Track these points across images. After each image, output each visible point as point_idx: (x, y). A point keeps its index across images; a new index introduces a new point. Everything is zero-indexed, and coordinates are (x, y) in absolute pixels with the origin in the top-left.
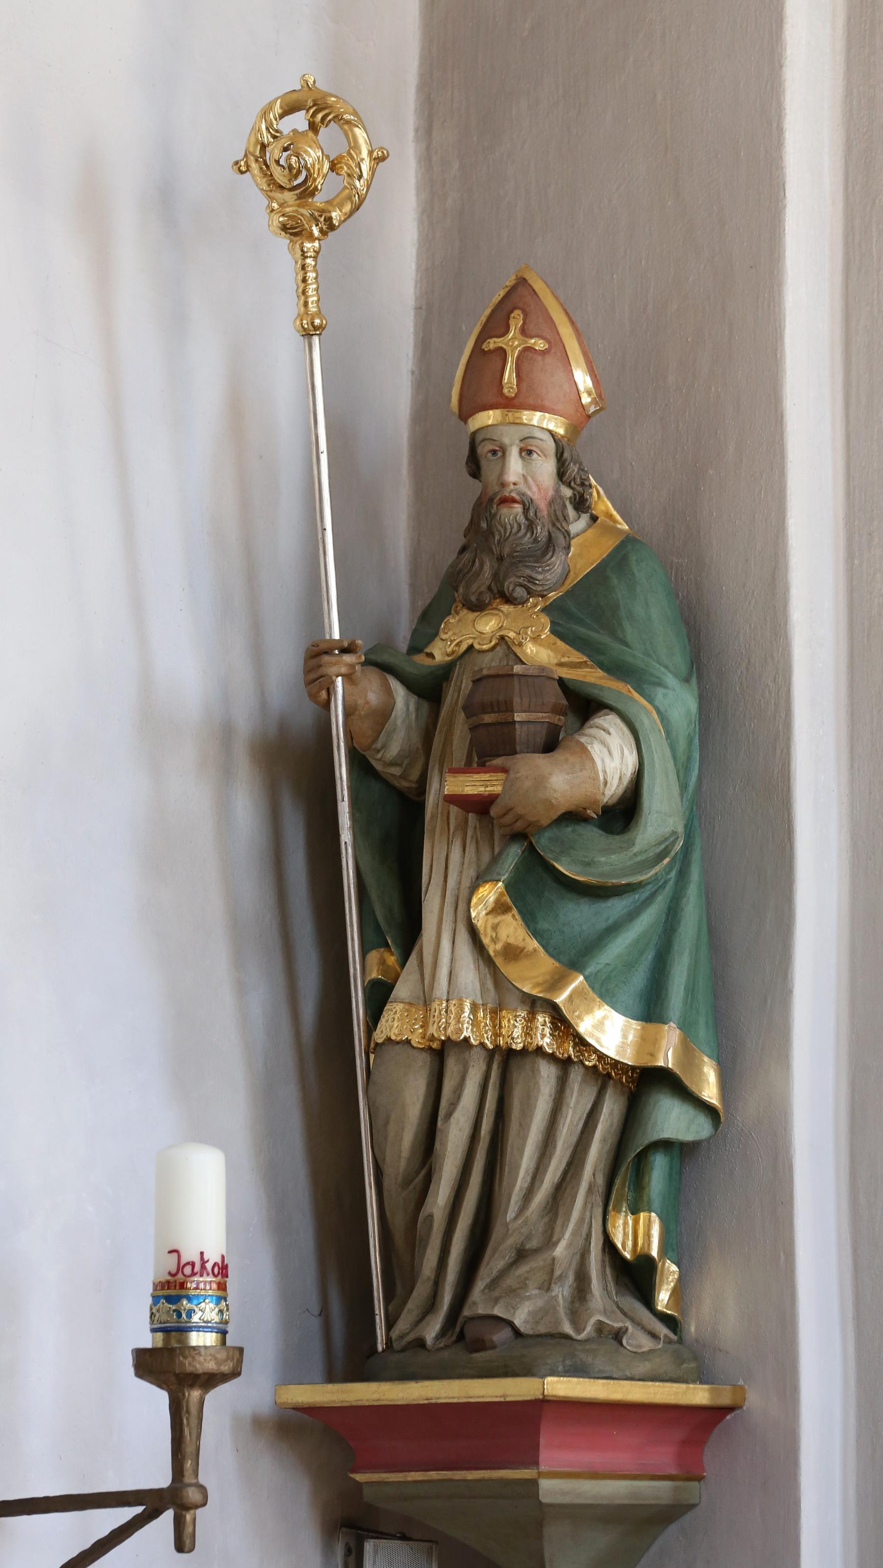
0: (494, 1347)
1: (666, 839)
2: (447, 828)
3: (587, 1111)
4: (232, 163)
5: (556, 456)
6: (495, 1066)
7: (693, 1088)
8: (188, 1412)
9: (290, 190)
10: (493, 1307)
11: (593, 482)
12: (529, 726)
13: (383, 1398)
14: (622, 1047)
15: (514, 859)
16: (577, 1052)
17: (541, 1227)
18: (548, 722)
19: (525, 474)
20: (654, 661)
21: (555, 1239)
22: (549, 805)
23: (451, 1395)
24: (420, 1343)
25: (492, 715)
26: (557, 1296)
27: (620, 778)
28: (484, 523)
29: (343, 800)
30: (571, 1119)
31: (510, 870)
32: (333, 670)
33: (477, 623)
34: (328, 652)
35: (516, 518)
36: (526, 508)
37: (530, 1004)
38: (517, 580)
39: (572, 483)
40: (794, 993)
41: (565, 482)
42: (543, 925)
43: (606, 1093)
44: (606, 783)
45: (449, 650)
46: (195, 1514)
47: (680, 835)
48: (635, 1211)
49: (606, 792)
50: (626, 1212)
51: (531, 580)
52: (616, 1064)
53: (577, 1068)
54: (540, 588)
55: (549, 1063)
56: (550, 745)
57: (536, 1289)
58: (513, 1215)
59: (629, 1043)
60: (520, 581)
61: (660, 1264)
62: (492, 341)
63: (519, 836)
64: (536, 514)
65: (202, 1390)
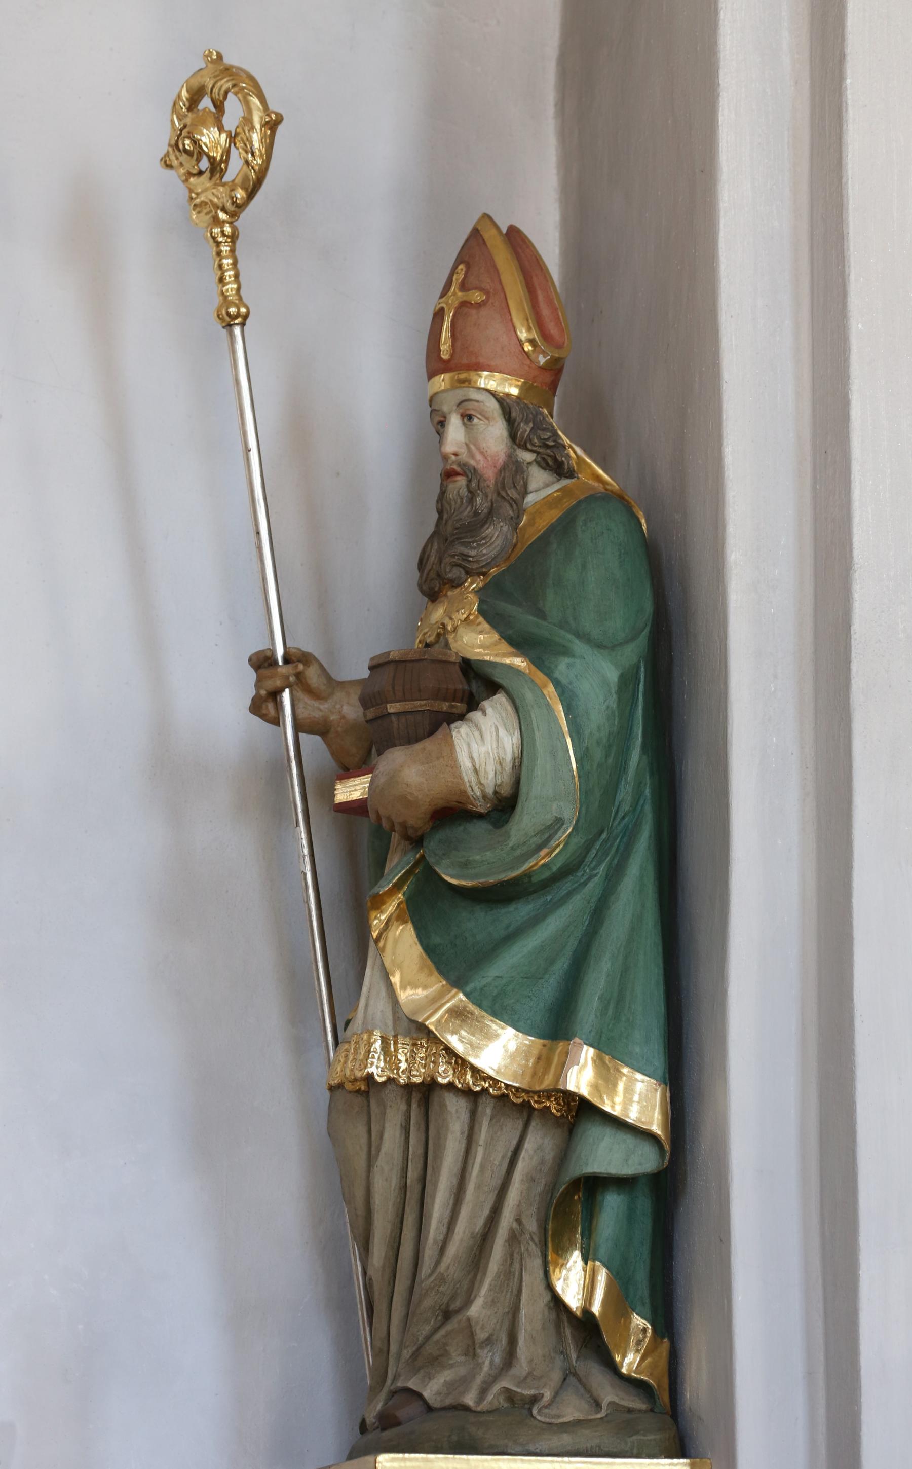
1: (549, 827)
5: (505, 417)
6: (414, 1106)
11: (566, 440)
19: (468, 442)
39: (529, 446)
40: (729, 993)
51: (464, 557)
53: (484, 1099)
54: (475, 566)
55: (456, 1096)
60: (454, 560)
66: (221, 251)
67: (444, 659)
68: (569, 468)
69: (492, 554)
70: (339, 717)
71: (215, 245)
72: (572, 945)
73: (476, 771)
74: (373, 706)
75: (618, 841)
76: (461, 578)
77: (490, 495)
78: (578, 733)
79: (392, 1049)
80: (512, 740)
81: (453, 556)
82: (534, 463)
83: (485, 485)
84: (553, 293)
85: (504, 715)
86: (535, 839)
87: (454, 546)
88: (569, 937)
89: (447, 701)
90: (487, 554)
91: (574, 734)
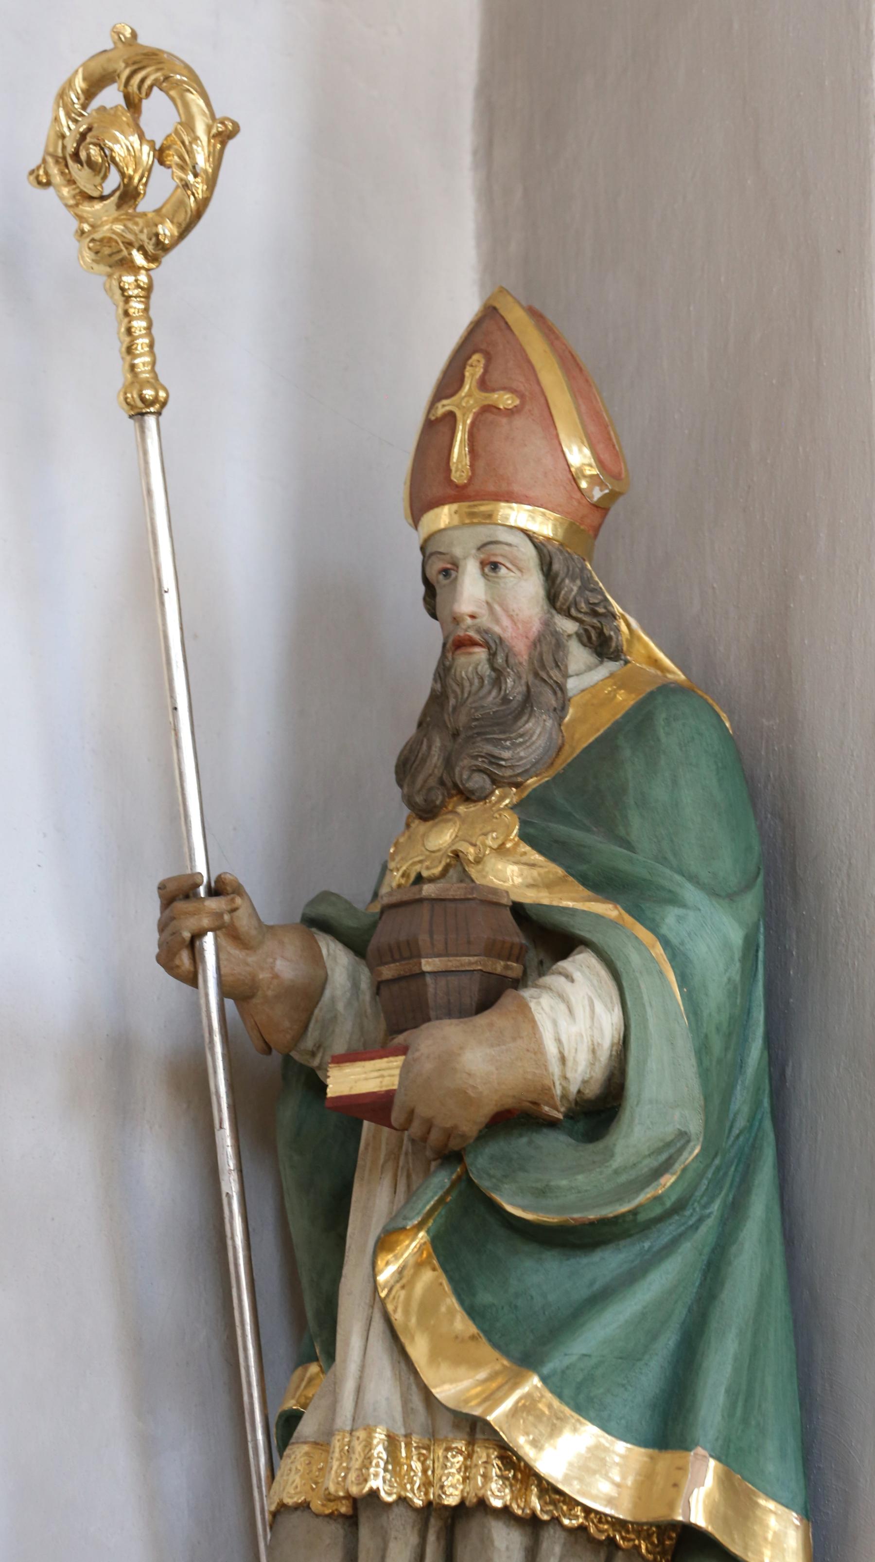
1: (668, 1145)
4: (26, 173)
5: (542, 569)
6: (432, 1537)
9: (102, 198)
11: (617, 608)
12: (449, 978)
15: (435, 1193)
16: (546, 1503)
18: (481, 970)
19: (490, 600)
20: (671, 868)
22: (465, 1099)
25: (392, 965)
27: (594, 1051)
29: (221, 1127)
37: (468, 1429)
39: (573, 612)
41: (561, 609)
42: (484, 1298)
47: (693, 1137)
51: (493, 760)
52: (619, 1524)
54: (509, 773)
55: (508, 1526)
64: (507, 661)
66: (131, 311)
67: (495, 900)
68: (617, 647)
69: (533, 758)
70: (271, 975)
71: (123, 299)
72: (680, 1313)
73: (563, 1060)
74: (394, 961)
75: (733, 1169)
76: (485, 789)
77: (524, 676)
78: (696, 1014)
79: (404, 1454)
80: (611, 1019)
81: (475, 757)
82: (574, 636)
83: (517, 661)
84: (600, 404)
85: (595, 982)
86: (646, 1162)
87: (474, 743)
88: (676, 1302)
89: (502, 960)
90: (526, 758)
91: (691, 1016)
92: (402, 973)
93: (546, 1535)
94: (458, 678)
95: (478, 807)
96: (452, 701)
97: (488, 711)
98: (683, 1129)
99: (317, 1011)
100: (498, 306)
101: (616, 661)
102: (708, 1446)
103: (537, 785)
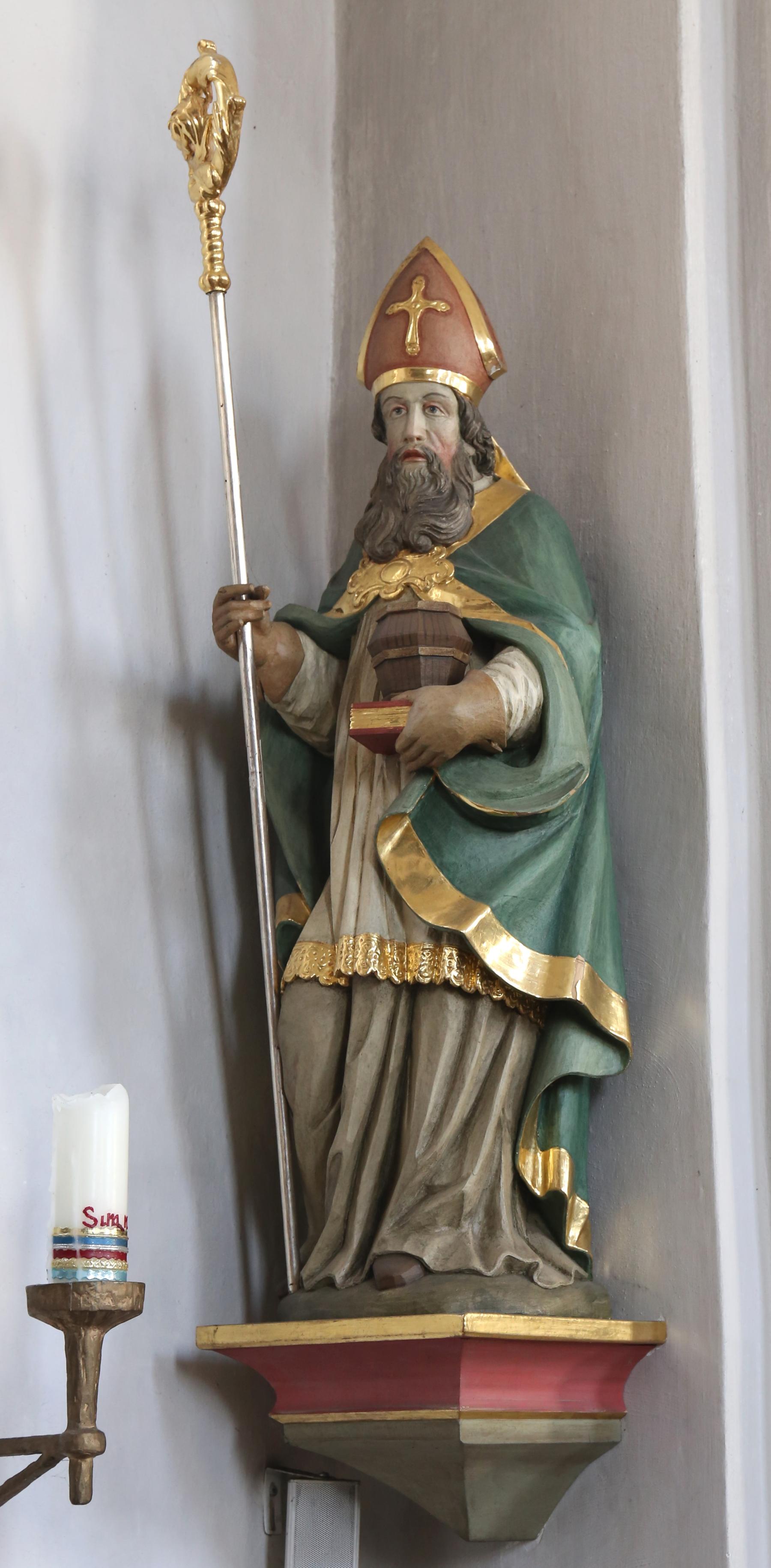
0: (403, 1284)
1: (572, 771)
2: (354, 773)
3: (495, 1047)
6: (403, 1003)
7: (602, 1023)
8: (85, 1352)
10: (402, 1245)
11: (495, 443)
13: (301, 1337)
14: (531, 976)
17: (450, 1163)
18: (453, 657)
19: (429, 430)
21: (464, 1174)
22: (455, 736)
23: (369, 1334)
24: (330, 1282)
26: (467, 1233)
27: (525, 711)
28: (389, 478)
30: (479, 1054)
31: (416, 803)
32: (239, 616)
33: (383, 574)
34: (236, 597)
35: (420, 471)
36: (430, 461)
38: (422, 529)
39: (475, 442)
43: (514, 1028)
44: (510, 715)
45: (357, 602)
46: (92, 1462)
47: (586, 768)
48: (544, 1147)
49: (511, 725)
50: (535, 1148)
51: (435, 529)
54: (444, 537)
55: (457, 998)
56: (456, 677)
57: (446, 1226)
58: (422, 1150)
59: (537, 976)
61: (570, 1201)
62: (395, 305)
63: (424, 771)
64: (439, 467)
65: (99, 1329)
69: (458, 529)
74: (397, 647)
81: (424, 526)
82: (471, 457)
90: (455, 529)
92: (404, 655)
93: (481, 1004)
94: (407, 475)
95: (423, 557)
96: (402, 491)
97: (429, 498)
98: (581, 763)
99: (297, 677)
100: (429, 248)
101: (488, 476)
102: (584, 955)
103: (459, 546)
